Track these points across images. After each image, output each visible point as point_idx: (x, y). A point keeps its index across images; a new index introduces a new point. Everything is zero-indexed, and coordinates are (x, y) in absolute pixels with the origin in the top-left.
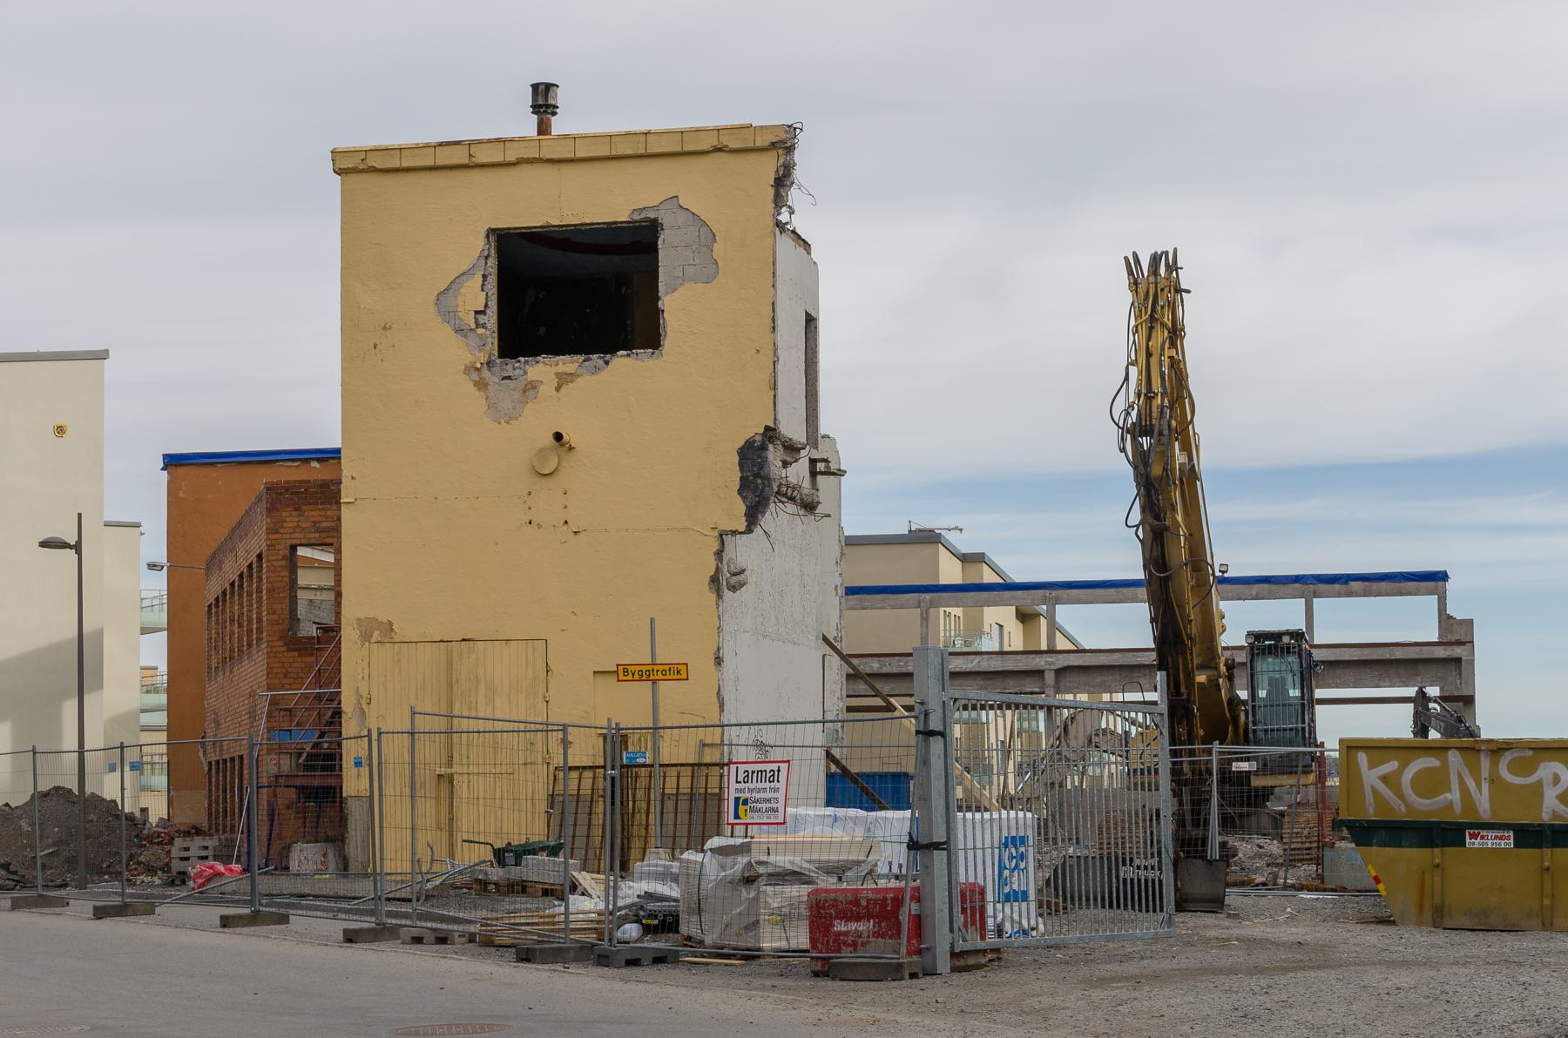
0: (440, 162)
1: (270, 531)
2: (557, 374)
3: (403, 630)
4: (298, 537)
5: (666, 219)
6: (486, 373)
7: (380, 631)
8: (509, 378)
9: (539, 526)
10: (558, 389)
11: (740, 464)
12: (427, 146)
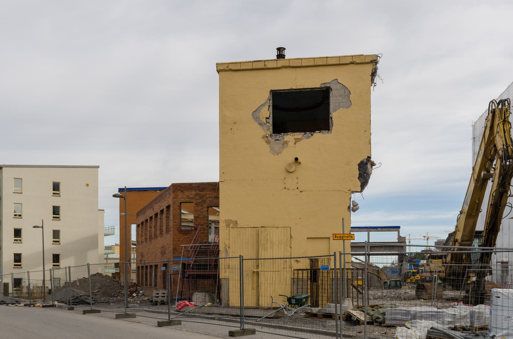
0: (254, 67)
1: (174, 198)
2: (295, 139)
3: (240, 224)
4: (182, 200)
5: (333, 86)
6: (270, 138)
7: (232, 224)
8: (278, 140)
9: (288, 189)
10: (295, 144)
11: (359, 169)
12: (250, 62)
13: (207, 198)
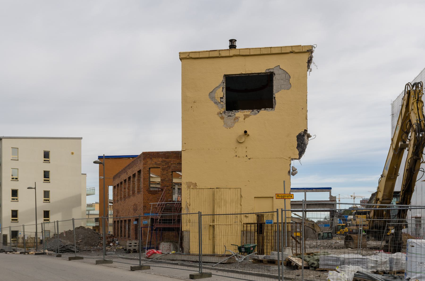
0: (210, 56)
1: (144, 164)
2: (244, 115)
3: (199, 185)
4: (151, 166)
5: (276, 72)
6: (223, 115)
7: (193, 186)
8: (230, 116)
9: (239, 157)
10: (244, 119)
11: (297, 140)
12: (207, 51)
13: (172, 164)
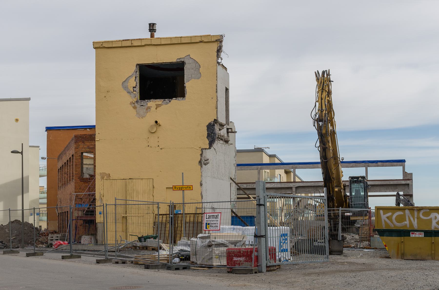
0: (123, 45)
1: (76, 148)
2: (156, 105)
3: (113, 176)
4: (83, 150)
5: (186, 61)
6: (136, 104)
7: (107, 176)
8: (143, 106)
9: (151, 147)
10: (156, 109)
11: (207, 130)
12: (120, 41)
